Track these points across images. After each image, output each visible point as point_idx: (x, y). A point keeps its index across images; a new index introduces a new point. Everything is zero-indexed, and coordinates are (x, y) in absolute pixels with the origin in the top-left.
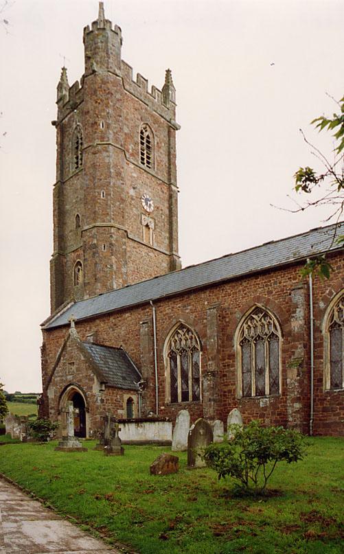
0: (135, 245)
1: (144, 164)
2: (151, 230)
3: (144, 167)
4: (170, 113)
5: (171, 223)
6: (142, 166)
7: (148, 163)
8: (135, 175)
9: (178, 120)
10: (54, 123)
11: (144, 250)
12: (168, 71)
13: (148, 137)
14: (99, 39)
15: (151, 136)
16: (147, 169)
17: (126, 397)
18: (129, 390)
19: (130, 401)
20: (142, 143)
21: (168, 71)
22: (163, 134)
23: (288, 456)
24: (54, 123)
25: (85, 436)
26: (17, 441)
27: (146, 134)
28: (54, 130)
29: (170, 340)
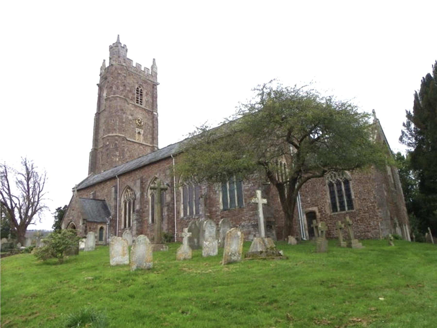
0: (131, 143)
1: (137, 103)
2: (141, 135)
3: (139, 105)
4: (154, 78)
5: (153, 134)
6: (137, 104)
7: (141, 102)
8: (132, 109)
9: (158, 81)
10: (97, 85)
11: (136, 146)
12: (154, 59)
13: (141, 90)
14: (117, 50)
15: (143, 89)
16: (140, 106)
17: (99, 226)
18: (101, 223)
19: (102, 228)
20: (138, 93)
21: (154, 59)
22: (150, 88)
23: (335, 148)
24: (97, 85)
25: (174, 241)
26: (343, 247)
27: (140, 89)
28: (97, 88)
29: (124, 195)
